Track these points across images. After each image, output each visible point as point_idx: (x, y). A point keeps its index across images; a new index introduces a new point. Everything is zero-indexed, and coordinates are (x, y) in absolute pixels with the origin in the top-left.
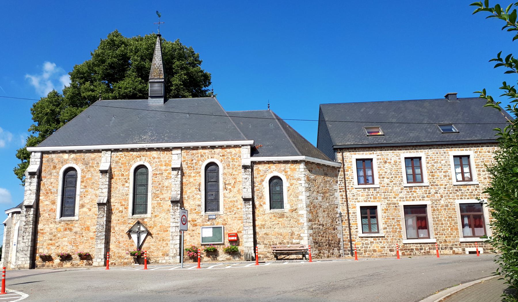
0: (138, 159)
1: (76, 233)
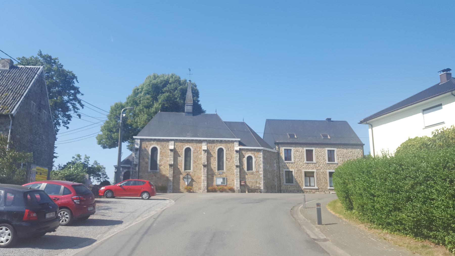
1: (158, 178)
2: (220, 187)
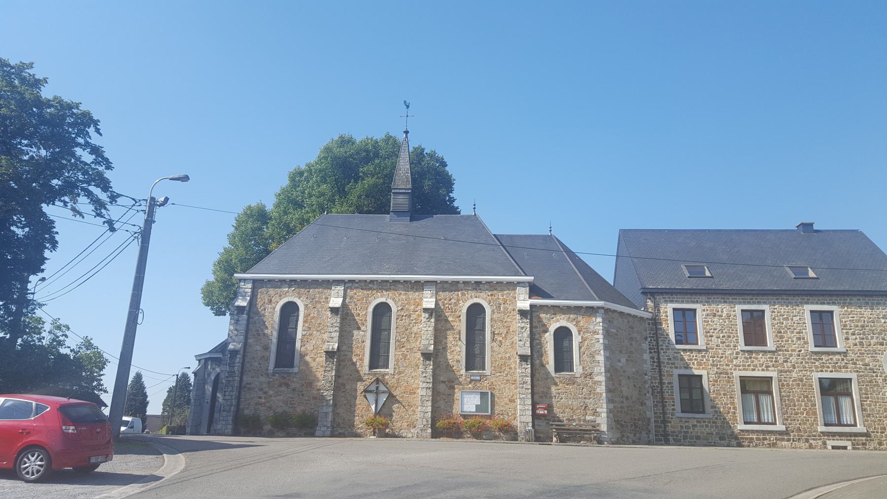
1: (294, 390)
2: (471, 421)
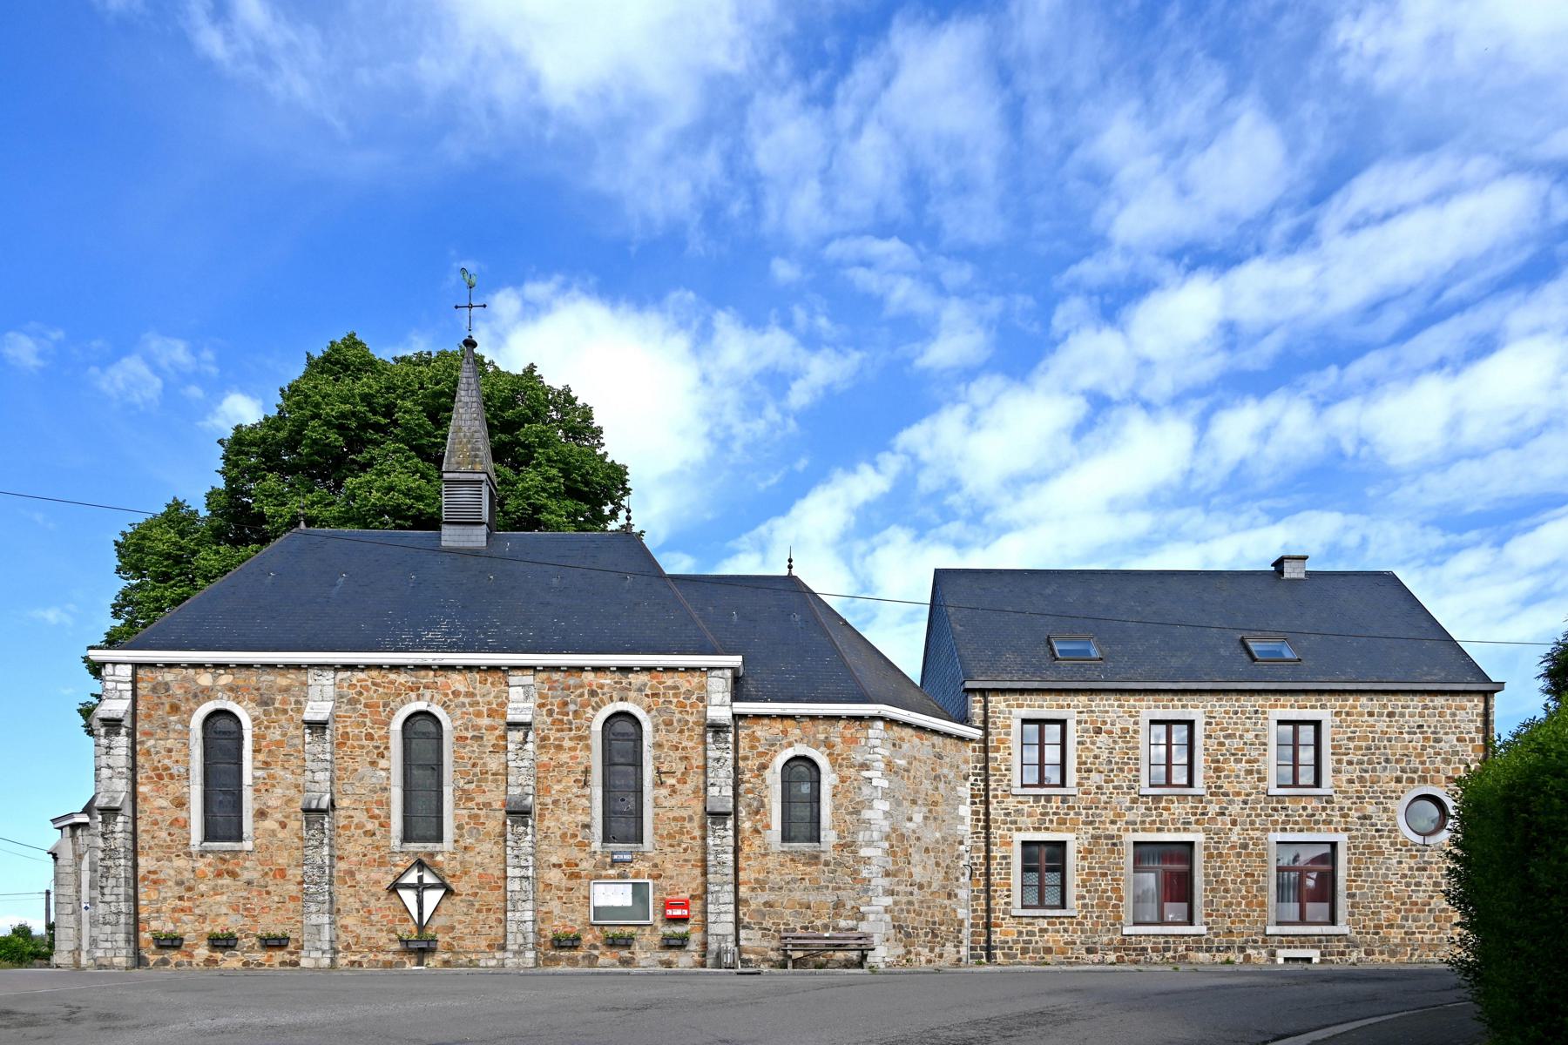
0: (413, 695)
1: (249, 883)
